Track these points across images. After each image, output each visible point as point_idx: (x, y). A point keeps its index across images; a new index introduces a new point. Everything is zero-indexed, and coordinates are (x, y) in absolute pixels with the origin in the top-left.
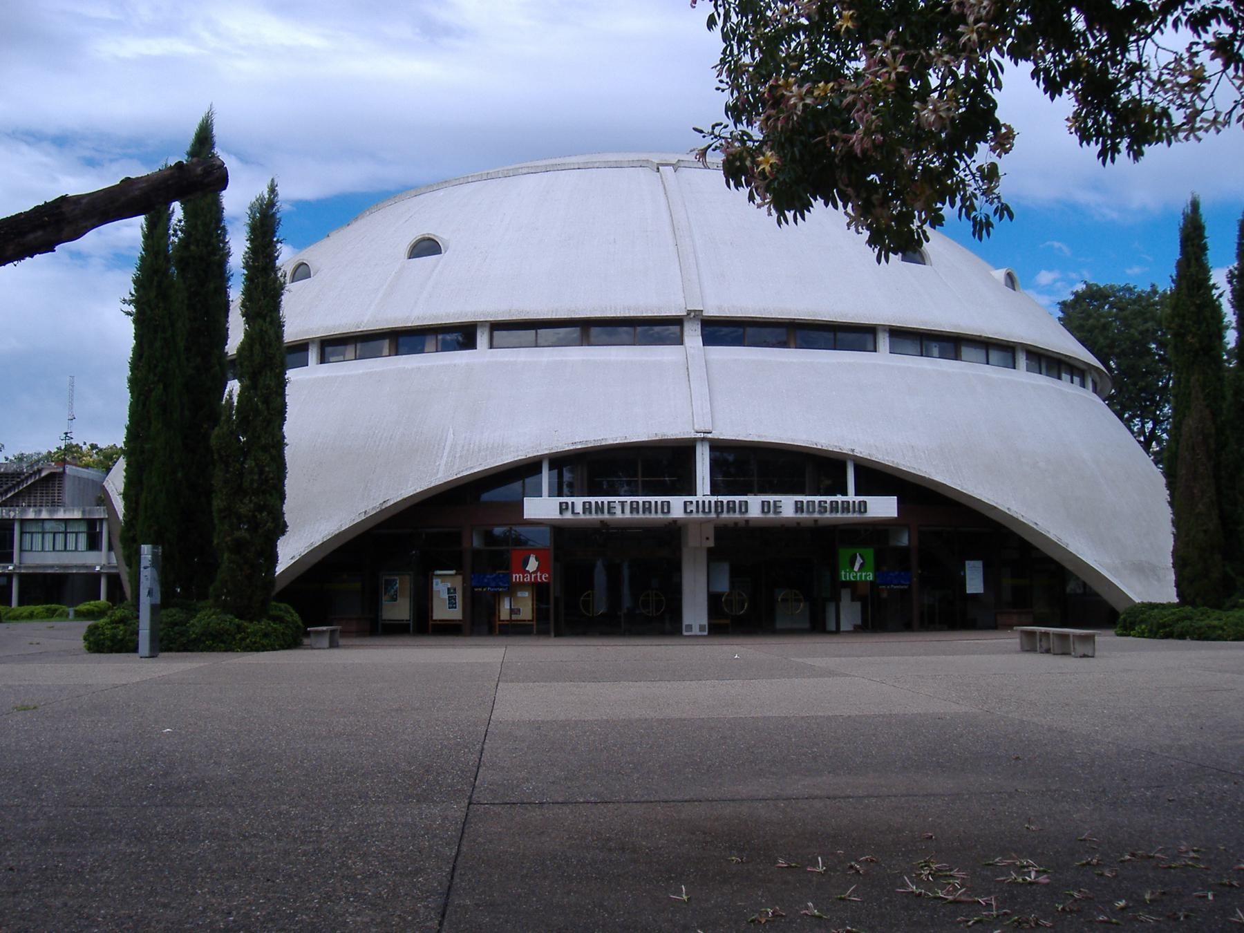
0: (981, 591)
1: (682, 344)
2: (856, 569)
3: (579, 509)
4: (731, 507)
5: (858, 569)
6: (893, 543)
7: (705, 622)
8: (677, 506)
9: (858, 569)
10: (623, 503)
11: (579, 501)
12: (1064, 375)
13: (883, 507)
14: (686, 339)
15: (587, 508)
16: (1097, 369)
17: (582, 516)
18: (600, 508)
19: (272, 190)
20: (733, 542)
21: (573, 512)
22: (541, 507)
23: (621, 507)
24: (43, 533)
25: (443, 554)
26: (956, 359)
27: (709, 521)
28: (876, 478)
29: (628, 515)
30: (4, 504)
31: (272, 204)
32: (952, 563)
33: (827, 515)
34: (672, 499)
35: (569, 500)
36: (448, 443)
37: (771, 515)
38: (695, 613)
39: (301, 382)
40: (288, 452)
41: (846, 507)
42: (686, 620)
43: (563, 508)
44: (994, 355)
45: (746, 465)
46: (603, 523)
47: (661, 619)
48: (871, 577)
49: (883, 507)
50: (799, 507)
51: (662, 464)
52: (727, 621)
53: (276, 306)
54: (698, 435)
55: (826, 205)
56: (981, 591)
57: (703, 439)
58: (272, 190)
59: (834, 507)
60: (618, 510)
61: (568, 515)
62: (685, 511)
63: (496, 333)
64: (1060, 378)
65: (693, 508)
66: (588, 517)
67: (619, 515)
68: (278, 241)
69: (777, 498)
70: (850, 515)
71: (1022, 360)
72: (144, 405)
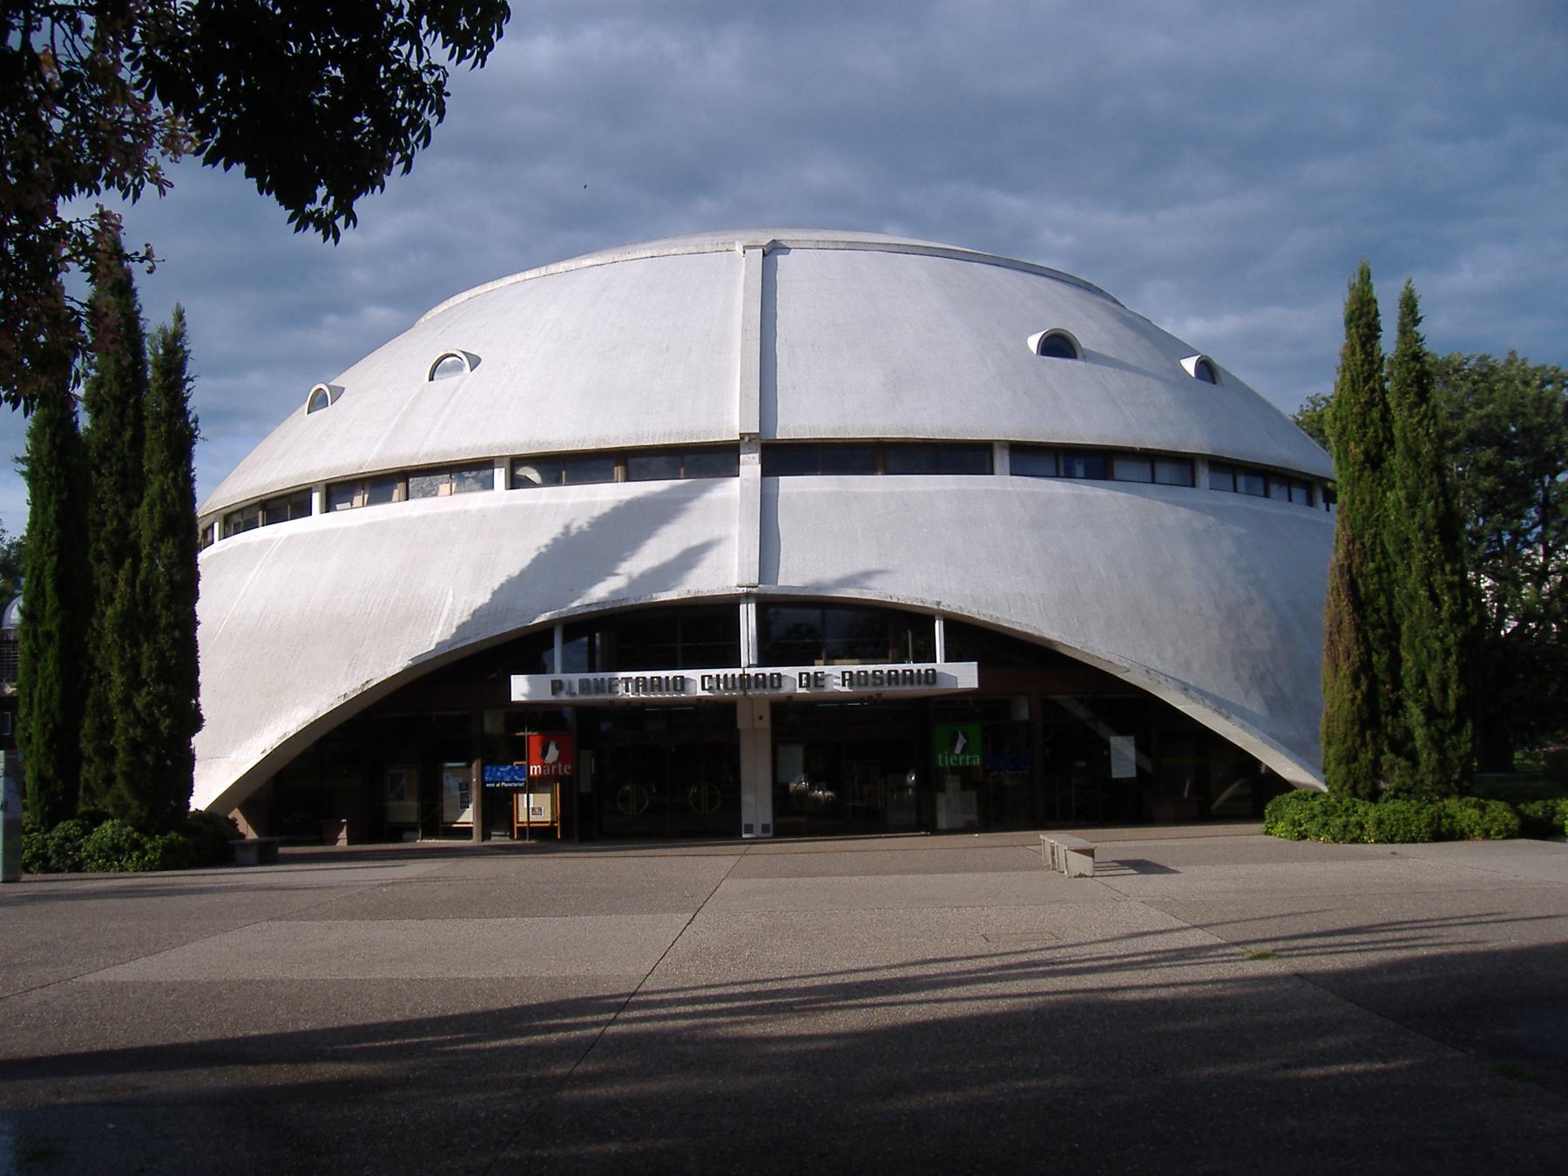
2: (958, 750)
3: (576, 689)
4: (599, 687)
5: (959, 752)
7: (769, 820)
9: (959, 752)
10: (627, 680)
11: (575, 678)
12: (1273, 488)
19: (180, 317)
20: (796, 720)
26: (1106, 478)
28: (970, 637)
31: (178, 336)
32: (1048, 740)
35: (565, 677)
36: (446, 610)
38: (756, 805)
40: (201, 634)
42: (746, 819)
44: (1163, 471)
45: (800, 624)
46: (612, 702)
47: (715, 822)
48: (977, 761)
52: (795, 820)
53: (188, 456)
54: (740, 590)
55: (291, 220)
58: (180, 317)
61: (564, 697)
63: (789, 485)
64: (1267, 495)
68: (188, 379)
71: (1203, 475)
72: (38, 579)
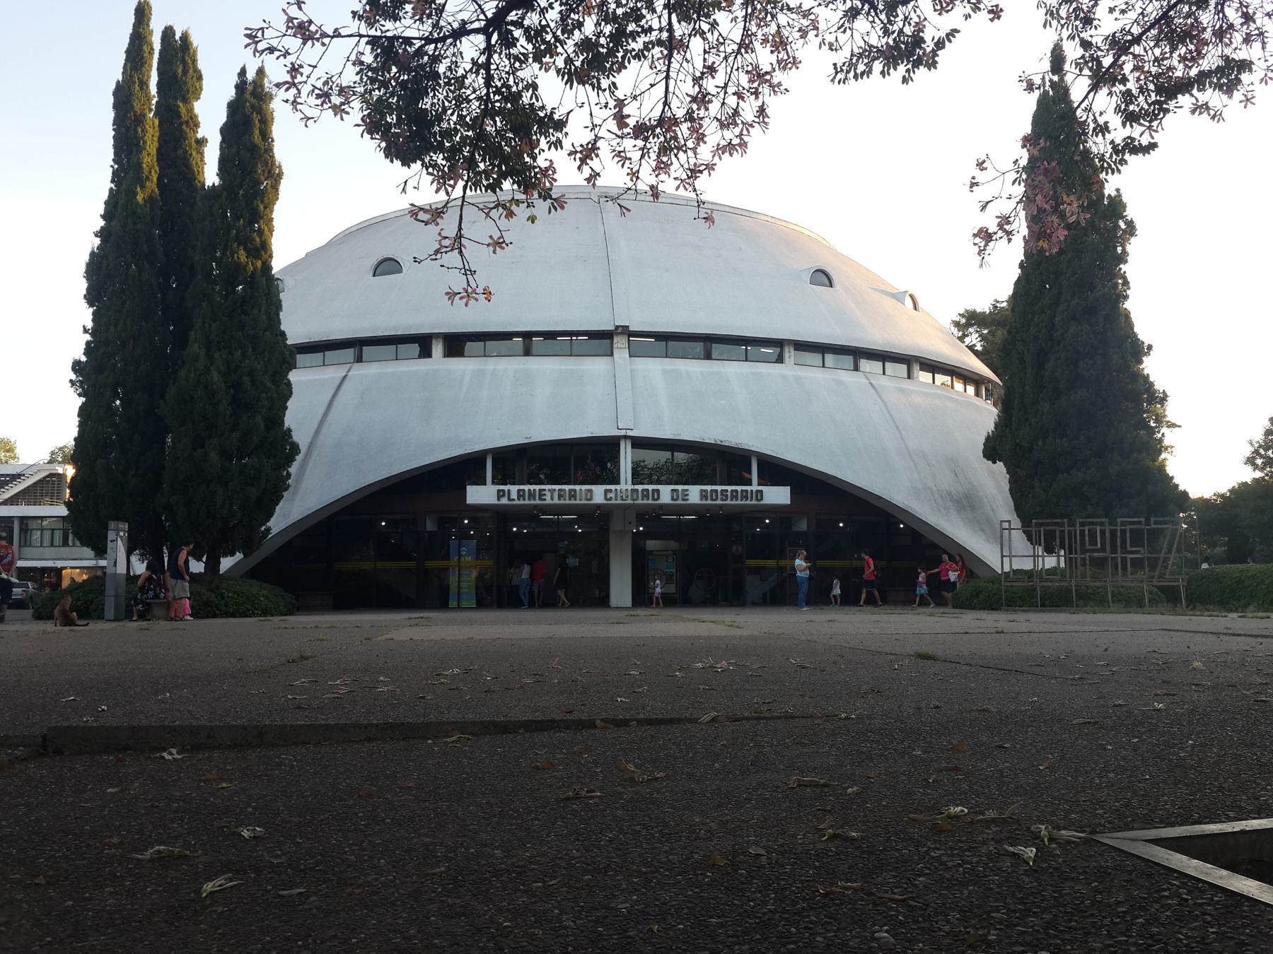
0: (469, 488)
1: (612, 355)
3: (514, 496)
6: (794, 529)
8: (598, 494)
10: (552, 491)
11: (514, 489)
13: (778, 495)
14: (615, 351)
15: (521, 494)
16: (990, 381)
17: (517, 502)
18: (532, 495)
21: (509, 499)
22: (481, 494)
23: (552, 494)
24: (42, 530)
25: (407, 534)
27: (629, 506)
28: (775, 471)
29: (556, 501)
30: (5, 503)
33: (729, 502)
34: (593, 487)
35: (505, 488)
37: (680, 502)
39: (308, 382)
41: (745, 495)
43: (500, 494)
49: (778, 495)
50: (704, 495)
51: (590, 457)
56: (469, 488)
57: (626, 437)
59: (734, 495)
60: (548, 497)
61: (504, 501)
62: (606, 498)
65: (612, 495)
66: (522, 502)
67: (548, 501)
69: (686, 487)
70: (1252, 566)
